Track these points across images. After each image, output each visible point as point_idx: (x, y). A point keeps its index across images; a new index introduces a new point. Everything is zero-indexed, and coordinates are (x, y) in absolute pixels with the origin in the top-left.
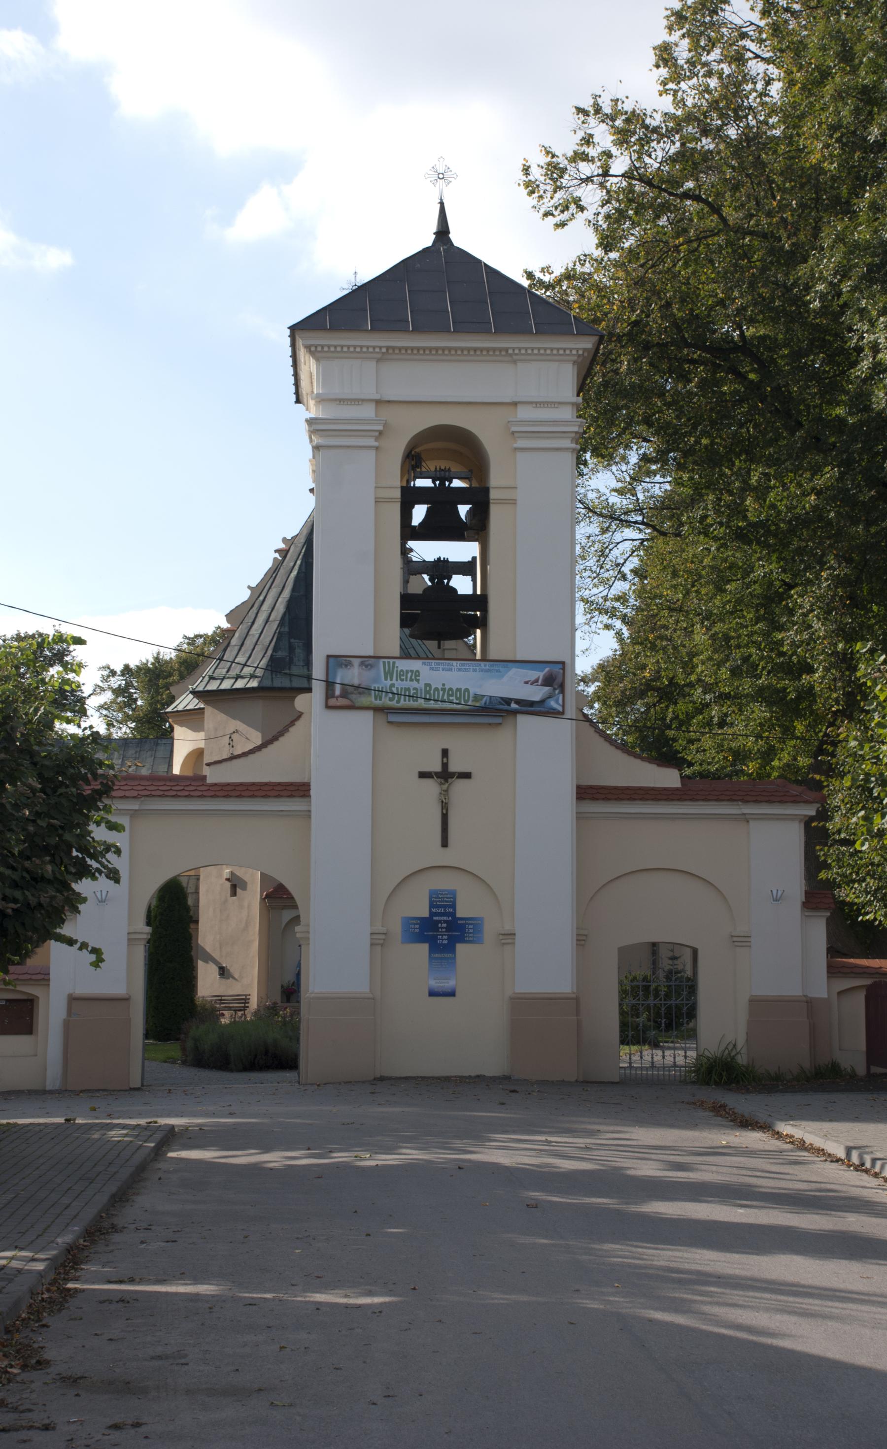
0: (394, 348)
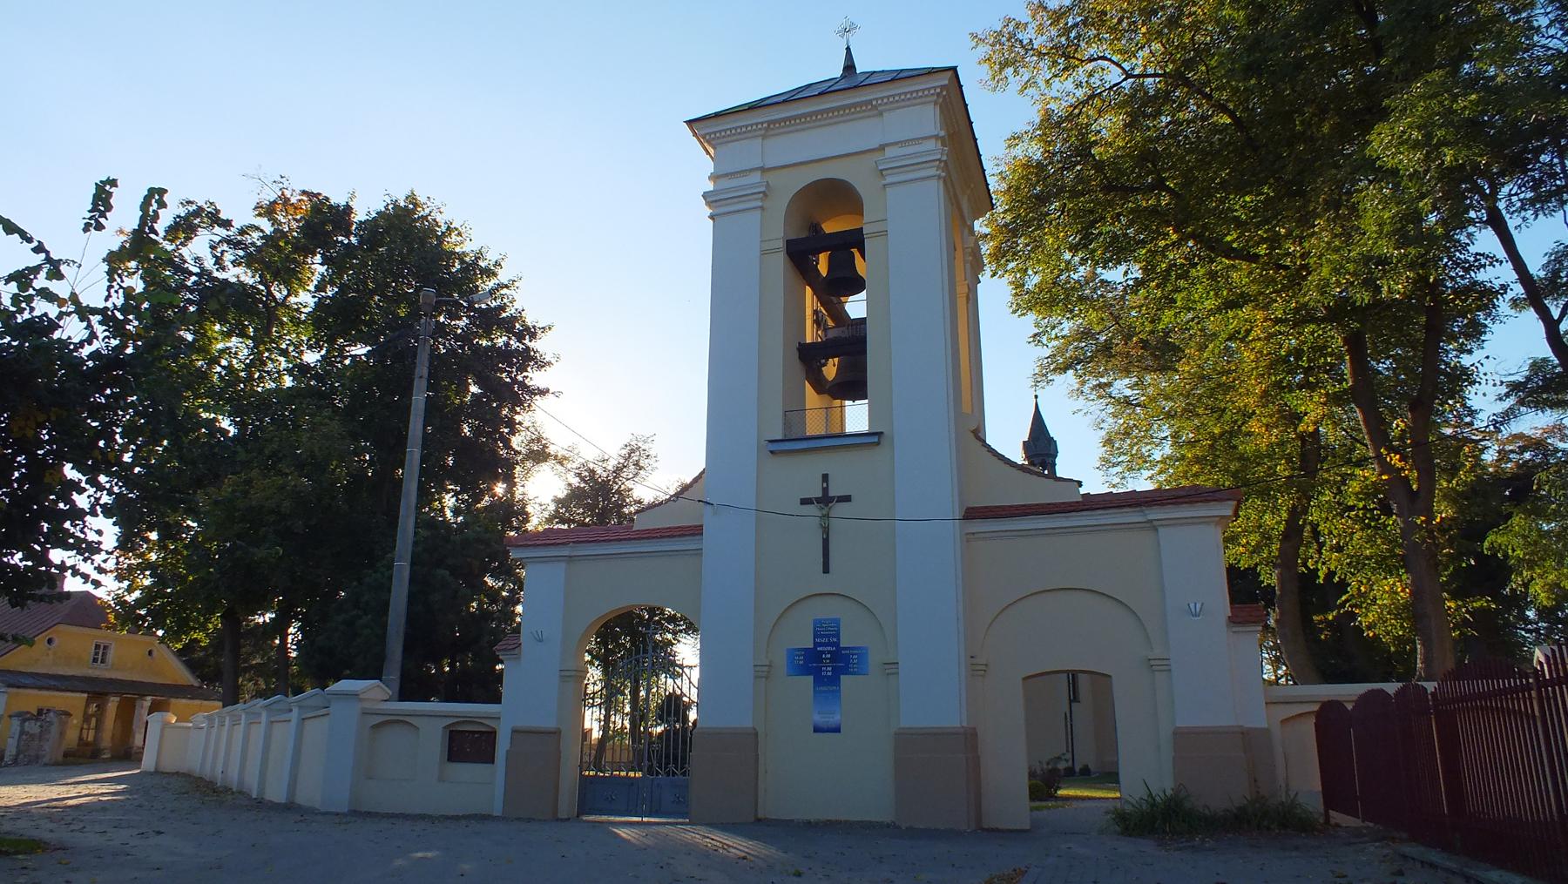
0: (774, 122)
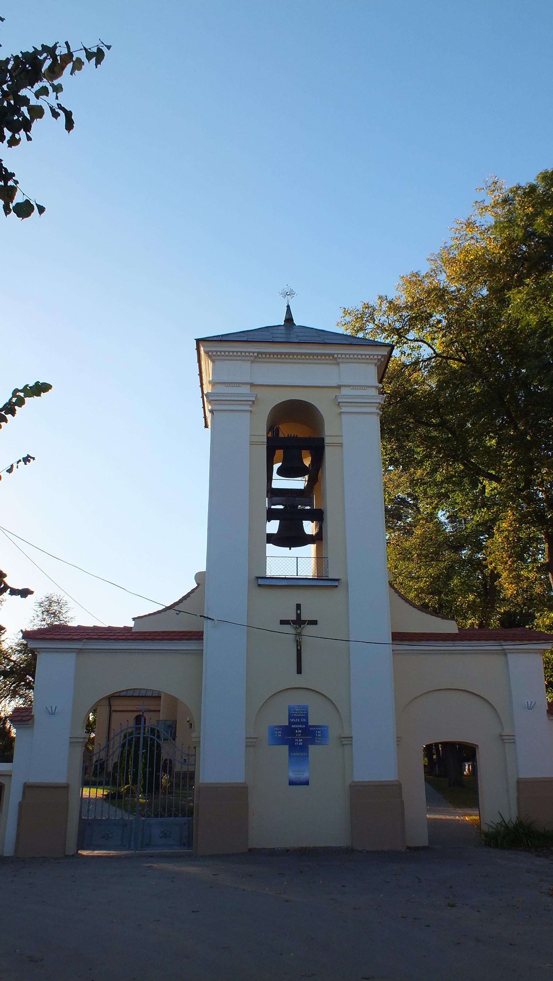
0: (262, 353)
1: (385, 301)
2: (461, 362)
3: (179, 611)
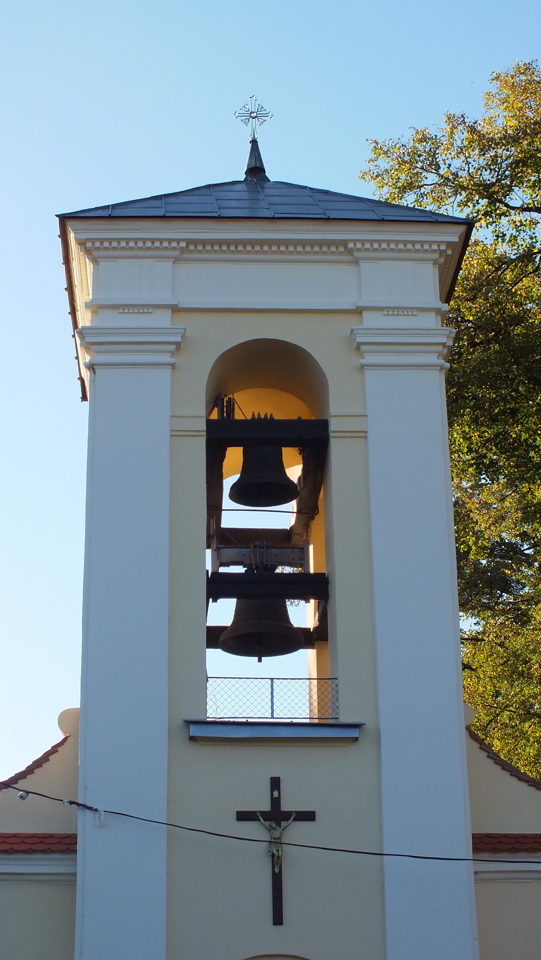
1: (461, 127)
2: (465, 253)
3: (26, 792)
